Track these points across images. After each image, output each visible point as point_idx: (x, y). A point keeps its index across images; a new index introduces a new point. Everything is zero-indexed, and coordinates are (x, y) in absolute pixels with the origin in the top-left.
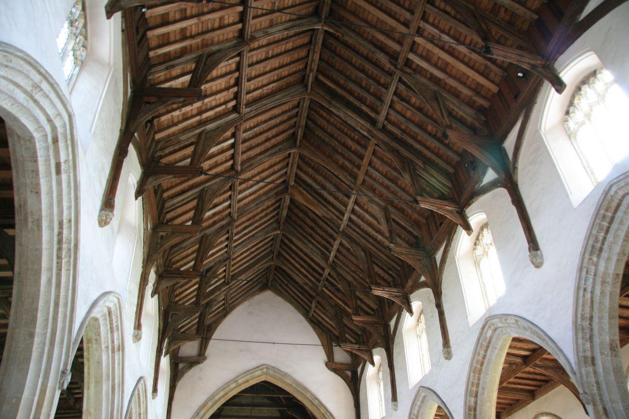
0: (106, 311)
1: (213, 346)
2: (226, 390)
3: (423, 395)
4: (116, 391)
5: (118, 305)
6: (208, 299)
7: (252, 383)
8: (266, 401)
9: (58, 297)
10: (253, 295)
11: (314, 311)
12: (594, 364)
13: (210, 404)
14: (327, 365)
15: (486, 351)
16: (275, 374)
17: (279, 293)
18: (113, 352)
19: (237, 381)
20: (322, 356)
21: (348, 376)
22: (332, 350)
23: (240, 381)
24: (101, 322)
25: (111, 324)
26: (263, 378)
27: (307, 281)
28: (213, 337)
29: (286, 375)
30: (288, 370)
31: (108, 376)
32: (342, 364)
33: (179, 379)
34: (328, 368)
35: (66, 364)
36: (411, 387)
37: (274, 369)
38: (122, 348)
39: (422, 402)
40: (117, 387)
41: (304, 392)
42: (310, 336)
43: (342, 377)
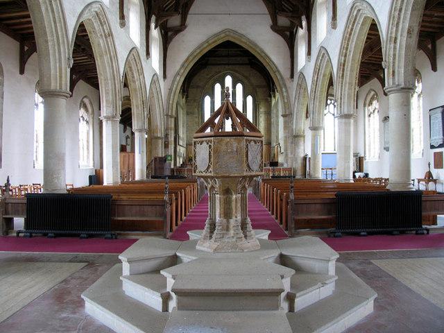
2: (202, 48)
7: (218, 43)
8: (239, 53)
9: (54, 18)
12: (395, 42)
13: (191, 58)
14: (272, 27)
15: (353, 25)
18: (106, 37)
20: (268, 21)
23: (210, 42)
25: (100, 21)
26: (225, 39)
28: (190, 12)
29: (242, 35)
30: (243, 32)
31: (106, 52)
35: (69, 54)
38: (110, 34)
40: (114, 57)
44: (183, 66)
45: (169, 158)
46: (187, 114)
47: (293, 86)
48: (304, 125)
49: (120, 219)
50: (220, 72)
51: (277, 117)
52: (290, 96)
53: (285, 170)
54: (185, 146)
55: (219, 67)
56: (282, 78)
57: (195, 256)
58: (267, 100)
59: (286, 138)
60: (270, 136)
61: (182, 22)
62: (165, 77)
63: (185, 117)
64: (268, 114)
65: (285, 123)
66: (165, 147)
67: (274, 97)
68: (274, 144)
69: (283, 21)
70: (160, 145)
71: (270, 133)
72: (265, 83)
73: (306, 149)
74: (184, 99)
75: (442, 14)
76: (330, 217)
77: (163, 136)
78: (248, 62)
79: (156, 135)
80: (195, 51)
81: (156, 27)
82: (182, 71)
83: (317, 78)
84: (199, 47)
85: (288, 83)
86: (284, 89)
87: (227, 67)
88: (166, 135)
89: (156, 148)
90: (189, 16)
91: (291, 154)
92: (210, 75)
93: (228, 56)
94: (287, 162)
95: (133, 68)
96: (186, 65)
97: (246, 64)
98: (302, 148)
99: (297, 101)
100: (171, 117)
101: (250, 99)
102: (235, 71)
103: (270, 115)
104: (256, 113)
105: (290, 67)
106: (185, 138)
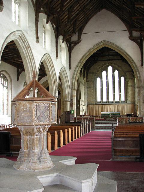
0: (18, 37)
1: (83, 36)
4: (32, 60)
5: (22, 34)
6: (76, 18)
7: (99, 48)
10: (98, 12)
11: (123, 15)
13: (84, 58)
17: (108, 9)
18: (27, 49)
20: (127, 34)
21: (139, 42)
22: (132, 32)
24: (18, 40)
27: (117, 3)
28: (83, 33)
29: (112, 44)
30: (113, 42)
32: (136, 37)
38: (29, 47)
40: (32, 59)
41: (120, 50)
42: (122, 27)
43: (136, 43)
45: (73, 112)
46: (88, 88)
49: (14, 145)
50: (105, 64)
53: (139, 118)
54: (86, 105)
55: (105, 62)
56: (136, 66)
60: (135, 99)
61: (78, 38)
62: (70, 68)
63: (86, 90)
65: (139, 91)
66: (71, 106)
69: (136, 34)
75: (13, 1)
76: (60, 162)
77: (70, 100)
78: (120, 58)
79: (65, 100)
81: (63, 42)
82: (79, 65)
84: (88, 51)
85: (140, 69)
88: (72, 100)
90: (82, 35)
92: (100, 66)
95: (48, 65)
96: (82, 61)
97: (120, 60)
100: (74, 90)
101: (122, 79)
102: (113, 63)
104: (126, 85)
106: (86, 101)
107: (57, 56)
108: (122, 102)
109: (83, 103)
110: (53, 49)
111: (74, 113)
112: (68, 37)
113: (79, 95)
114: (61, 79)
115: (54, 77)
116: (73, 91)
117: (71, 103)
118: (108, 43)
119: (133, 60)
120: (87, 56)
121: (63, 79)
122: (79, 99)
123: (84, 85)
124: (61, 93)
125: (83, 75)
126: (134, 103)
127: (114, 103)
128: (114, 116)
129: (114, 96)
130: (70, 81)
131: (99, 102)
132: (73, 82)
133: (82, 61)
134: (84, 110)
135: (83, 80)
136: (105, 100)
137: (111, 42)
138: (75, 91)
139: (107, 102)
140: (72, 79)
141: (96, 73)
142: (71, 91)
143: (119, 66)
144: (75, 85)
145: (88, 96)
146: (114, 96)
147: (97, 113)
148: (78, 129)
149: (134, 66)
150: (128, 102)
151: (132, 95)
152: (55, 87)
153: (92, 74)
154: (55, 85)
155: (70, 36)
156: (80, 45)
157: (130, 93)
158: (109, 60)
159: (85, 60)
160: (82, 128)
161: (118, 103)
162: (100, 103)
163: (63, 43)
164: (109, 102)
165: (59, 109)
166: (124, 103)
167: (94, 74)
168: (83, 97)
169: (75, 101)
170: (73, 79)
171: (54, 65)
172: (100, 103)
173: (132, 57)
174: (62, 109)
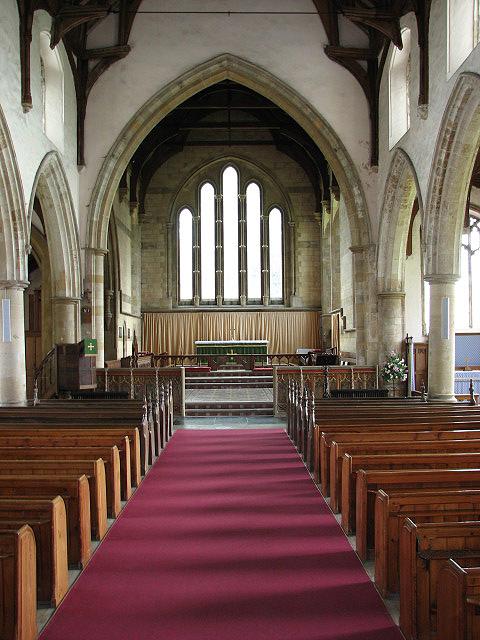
3: (466, 87)
7: (205, 85)
13: (141, 120)
16: (241, 68)
19: (181, 82)
20: (321, 36)
23: (185, 83)
28: (140, 10)
29: (259, 69)
30: (262, 61)
33: (91, 86)
34: (329, 56)
36: (449, 76)
37: (241, 60)
39: (465, 101)
44: (123, 135)
46: (144, 246)
47: (375, 183)
48: (407, 272)
50: (211, 159)
51: (337, 252)
52: (370, 205)
53: (362, 371)
54: (139, 314)
56: (350, 163)
57: (183, 436)
58: (312, 219)
59: (359, 302)
62: (81, 161)
63: (138, 255)
64: (316, 245)
67: (329, 210)
68: (328, 310)
70: (71, 317)
71: (321, 286)
72: (310, 184)
73: (411, 322)
74: (135, 215)
77: (78, 296)
78: (272, 139)
79: (60, 294)
80: (150, 103)
81: (53, 44)
82: (121, 148)
83: (448, 155)
84: (159, 95)
85: (365, 175)
86: (356, 191)
87: (227, 148)
88: (86, 295)
89: (61, 324)
90: (139, 22)
91: (373, 336)
92: (194, 165)
93: (228, 123)
94: (364, 353)
96: (130, 135)
97: (270, 143)
98: (398, 321)
99: (386, 215)
100: (97, 252)
101: (276, 216)
103: (320, 250)
105: (368, 139)
106: (139, 298)
107: (26, 98)
108: (272, 303)
109: (127, 307)
110: (8, 59)
111: (95, 351)
112: (76, 24)
113: (114, 273)
114: (44, 205)
115: (10, 193)
116: (93, 257)
117: (82, 309)
118: (240, 64)
119: (338, 140)
120: (156, 111)
121: (52, 206)
122: (114, 289)
123: (132, 237)
124: (42, 266)
125: (128, 196)
126: (316, 309)
127: (241, 305)
128: (250, 357)
129: (243, 279)
130: (80, 214)
131: (186, 303)
132: (91, 222)
133: (130, 135)
134: (131, 335)
135: (128, 219)
136: (208, 292)
137: (253, 60)
138: (101, 258)
139: (215, 303)
140: (91, 206)
141: (177, 191)
142: (83, 258)
143: (262, 167)
144: (99, 231)
145: (145, 280)
146: (243, 279)
147: (177, 348)
148: (132, 444)
149: (344, 163)
150: (296, 303)
151: (309, 276)
152: (16, 238)
153: (161, 196)
154: (15, 230)
155: (84, 20)
156: (123, 68)
157: (303, 269)
158: (230, 143)
159: (160, 112)
160: (146, 436)
161: (212, 307)
162: (192, 308)
163: (52, 46)
164: (224, 303)
165: (33, 331)
166: (281, 307)
167: (170, 195)
168: (127, 285)
169: (99, 301)
170: (93, 209)
171: (12, 134)
172: (192, 308)
173: (337, 129)
174: (44, 334)
